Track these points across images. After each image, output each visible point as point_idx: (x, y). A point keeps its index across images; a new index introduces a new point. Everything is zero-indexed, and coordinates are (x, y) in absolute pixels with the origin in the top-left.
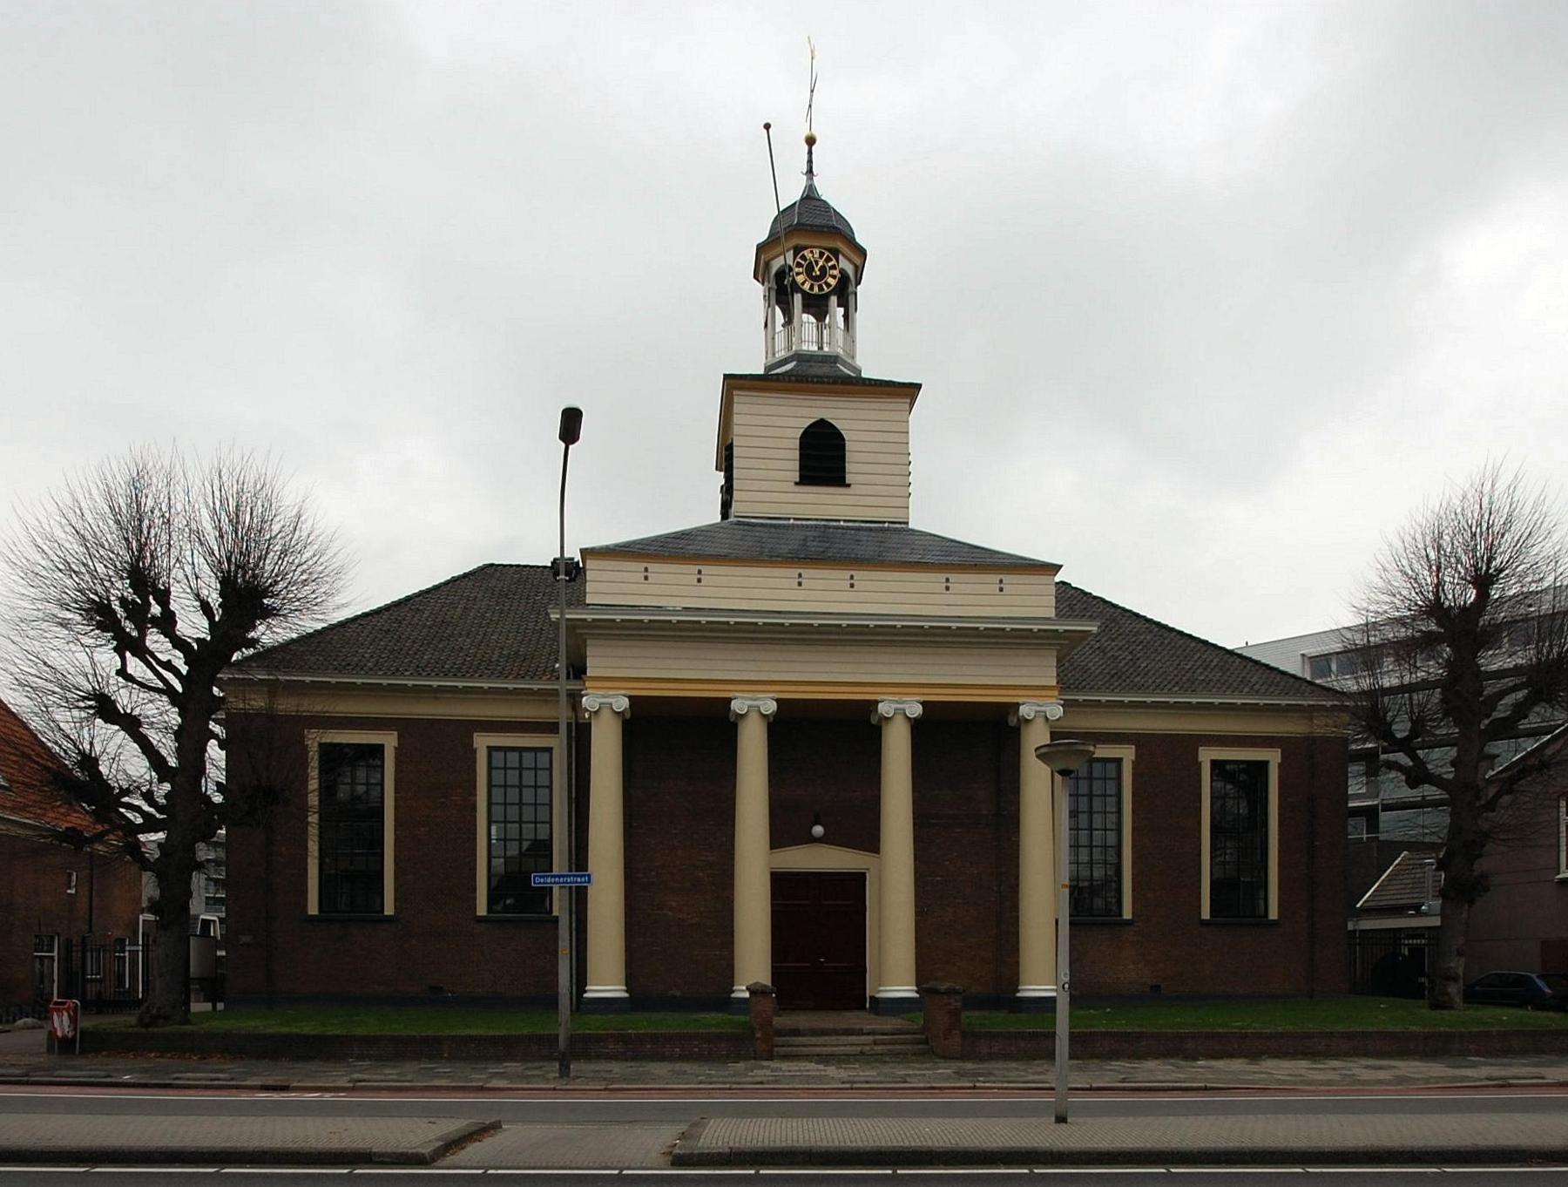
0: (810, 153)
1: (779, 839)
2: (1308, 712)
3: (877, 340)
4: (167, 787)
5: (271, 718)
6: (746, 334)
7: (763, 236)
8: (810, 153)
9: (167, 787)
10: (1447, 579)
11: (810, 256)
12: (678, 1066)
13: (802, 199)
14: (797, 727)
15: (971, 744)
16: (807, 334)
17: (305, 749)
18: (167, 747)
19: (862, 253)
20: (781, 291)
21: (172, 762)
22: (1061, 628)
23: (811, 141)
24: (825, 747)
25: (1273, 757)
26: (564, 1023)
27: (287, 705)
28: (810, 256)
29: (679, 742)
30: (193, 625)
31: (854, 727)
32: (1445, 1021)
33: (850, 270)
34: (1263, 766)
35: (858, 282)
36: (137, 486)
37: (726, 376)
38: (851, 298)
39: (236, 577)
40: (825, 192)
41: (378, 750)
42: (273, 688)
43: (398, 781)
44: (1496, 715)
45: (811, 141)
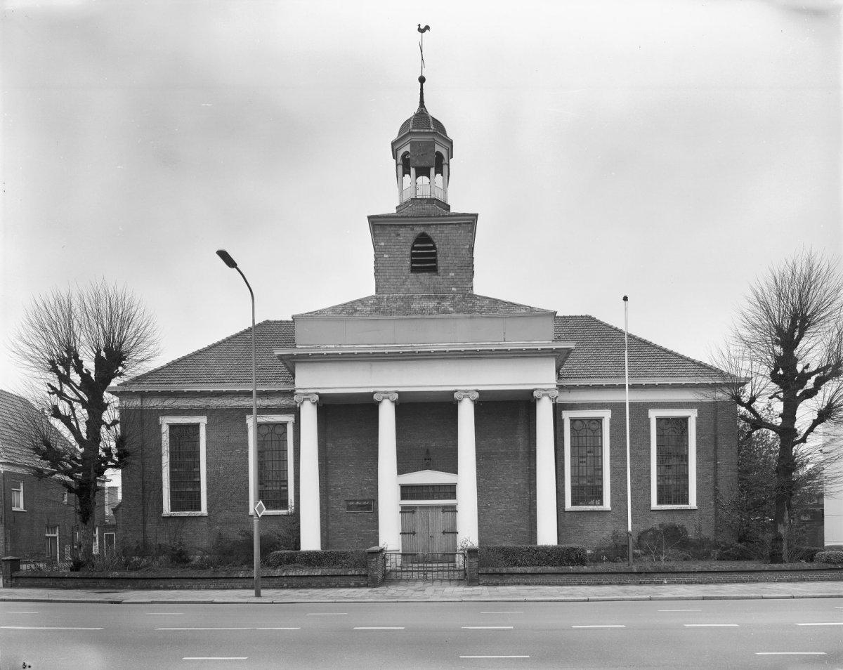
0: (422, 89)
1: (402, 469)
2: (714, 387)
3: (462, 190)
5: (141, 411)
6: (387, 192)
7: (395, 136)
8: (422, 89)
11: (424, 147)
12: (300, 590)
13: (416, 115)
15: (507, 415)
17: (160, 427)
18: (83, 428)
19: (451, 143)
20: (405, 165)
21: (84, 435)
22: (554, 347)
23: (422, 80)
25: (692, 415)
28: (424, 147)
29: (347, 418)
30: (89, 365)
31: (445, 407)
32: (783, 566)
35: (451, 155)
36: (807, 279)
37: (369, 217)
38: (445, 168)
39: (783, 326)
40: (432, 111)
41: (599, 421)
42: (143, 395)
43: (208, 442)
45: (422, 80)
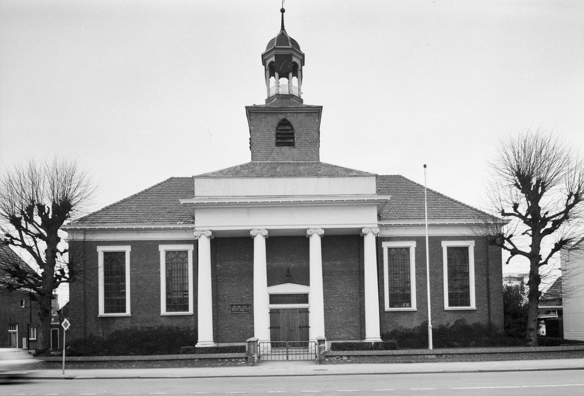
0: (283, 15)
1: (271, 282)
3: (311, 88)
4: (42, 270)
5: (84, 242)
6: (259, 89)
8: (283, 15)
9: (42, 270)
10: (246, 171)
14: (330, 240)
15: (344, 246)
16: (283, 85)
18: (43, 258)
23: (283, 11)
24: (288, 248)
26: (560, 319)
27: (90, 237)
29: (231, 248)
31: (244, 241)
33: (298, 62)
34: (465, 249)
38: (299, 72)
40: (290, 33)
42: (85, 231)
44: (547, 227)
45: (283, 11)
